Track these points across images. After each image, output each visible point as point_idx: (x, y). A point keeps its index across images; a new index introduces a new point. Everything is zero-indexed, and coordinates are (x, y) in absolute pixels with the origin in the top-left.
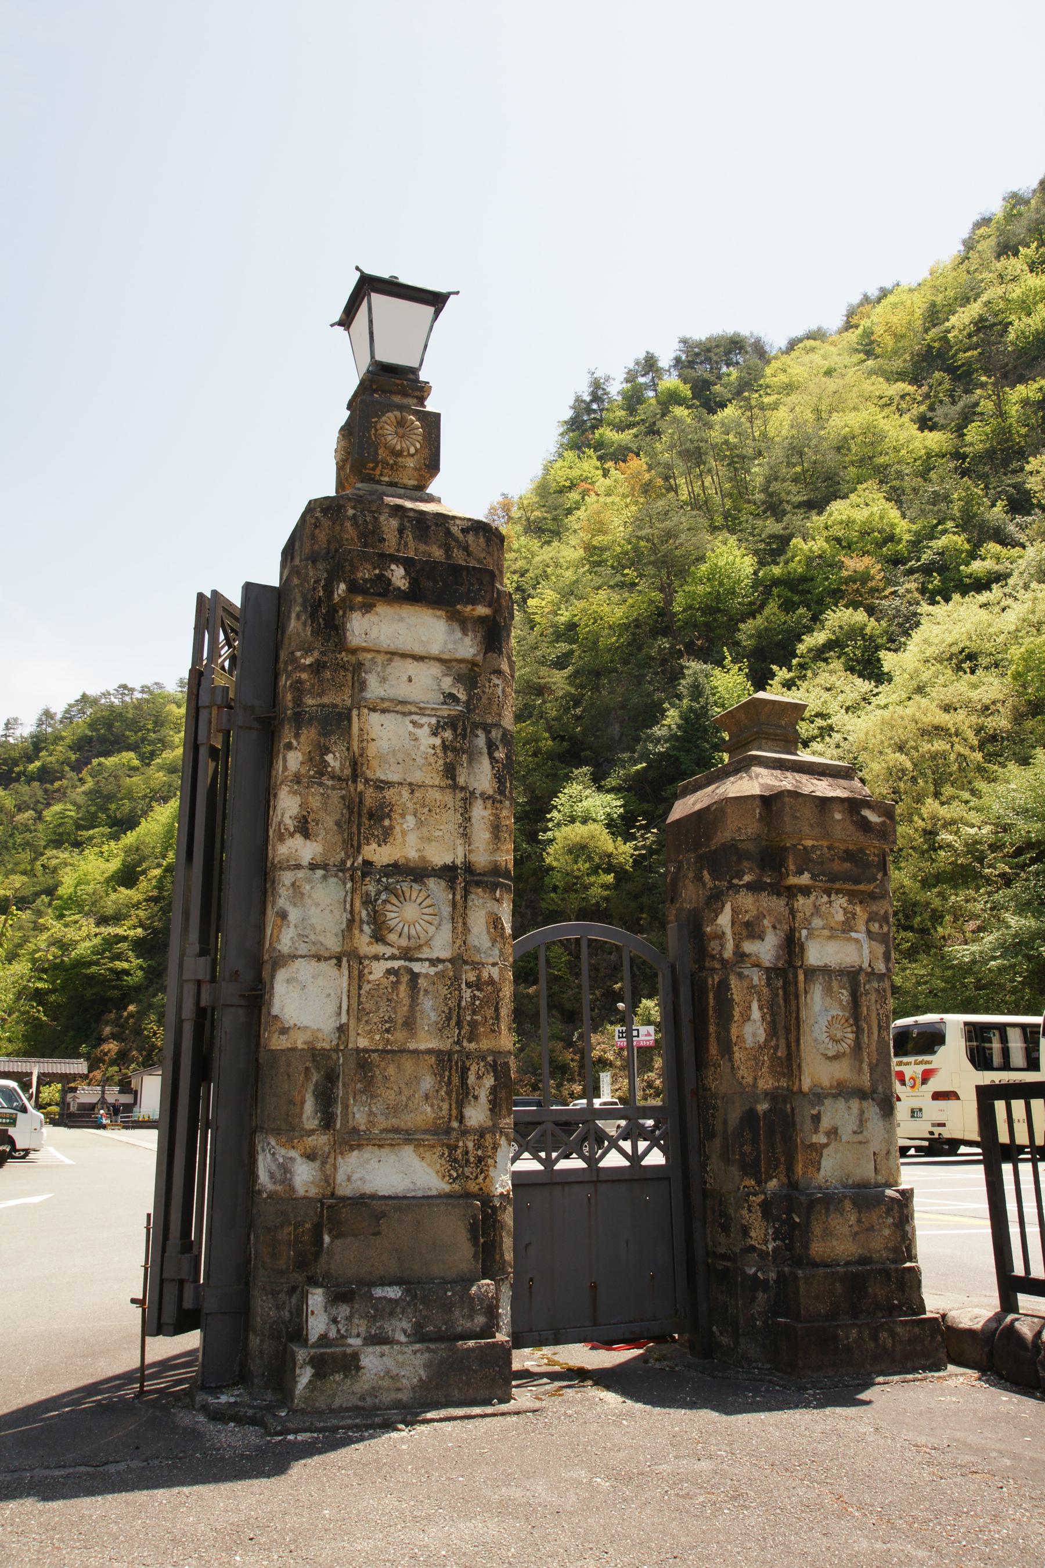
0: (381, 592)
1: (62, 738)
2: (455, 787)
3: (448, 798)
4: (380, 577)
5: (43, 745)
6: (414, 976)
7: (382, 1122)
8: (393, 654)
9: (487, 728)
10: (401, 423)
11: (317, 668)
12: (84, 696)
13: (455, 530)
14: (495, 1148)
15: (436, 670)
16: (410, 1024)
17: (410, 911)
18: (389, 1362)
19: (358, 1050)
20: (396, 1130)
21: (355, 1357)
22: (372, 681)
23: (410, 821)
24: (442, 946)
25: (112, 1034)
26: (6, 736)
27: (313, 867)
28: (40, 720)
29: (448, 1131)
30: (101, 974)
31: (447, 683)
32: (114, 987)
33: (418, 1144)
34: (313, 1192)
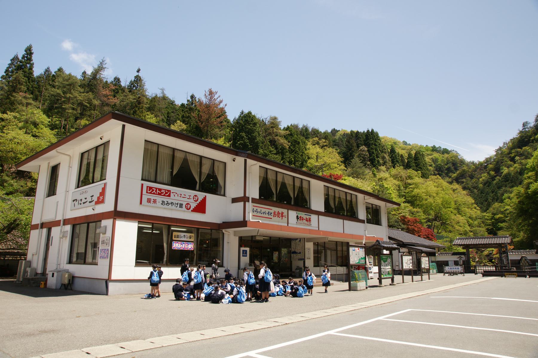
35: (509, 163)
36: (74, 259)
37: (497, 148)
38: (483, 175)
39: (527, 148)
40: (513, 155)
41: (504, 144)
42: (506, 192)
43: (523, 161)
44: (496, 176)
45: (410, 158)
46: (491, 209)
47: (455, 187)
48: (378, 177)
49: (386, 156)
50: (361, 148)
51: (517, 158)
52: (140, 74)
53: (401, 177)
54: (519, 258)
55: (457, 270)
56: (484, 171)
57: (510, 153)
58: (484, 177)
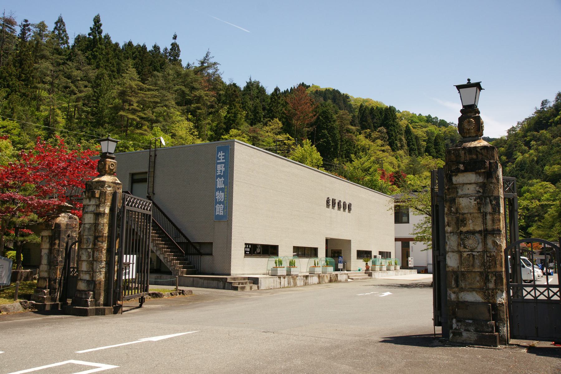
0: (458, 171)
2: (481, 212)
3: (479, 215)
4: (458, 168)
6: (474, 255)
7: (468, 287)
8: (464, 184)
9: (489, 197)
10: (469, 122)
11: (448, 189)
13: (478, 150)
14: (496, 293)
15: (474, 186)
16: (473, 266)
17: (470, 241)
18: (468, 335)
19: (462, 271)
20: (471, 288)
21: (461, 333)
22: (460, 191)
23: (471, 221)
24: (480, 248)
26: (543, 108)
27: (451, 233)
28: (557, 98)
29: (483, 289)
31: (477, 188)
33: (476, 292)
34: (455, 300)
35: (524, 147)
37: (509, 127)
39: (544, 132)
40: (528, 139)
41: (518, 124)
43: (540, 147)
44: (507, 162)
45: (430, 142)
48: (147, 73)
51: (533, 143)
52: (178, 41)
57: (525, 136)
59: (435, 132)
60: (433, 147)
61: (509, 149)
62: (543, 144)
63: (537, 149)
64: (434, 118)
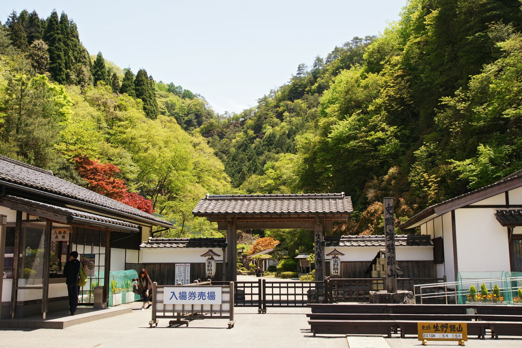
1: (327, 70)
5: (318, 75)
12: (336, 48)
25: (376, 196)
30: (360, 146)
32: (373, 157)
35: (276, 120)
36: (264, 261)
38: (237, 134)
39: (299, 101)
41: (271, 93)
42: (269, 158)
43: (294, 119)
44: (255, 138)
46: (246, 183)
47: (196, 140)
49: (84, 68)
50: (36, 42)
51: (286, 114)
53: (105, 104)
54: (370, 257)
55: (207, 303)
56: (241, 128)
58: (239, 137)
59: (177, 104)
60: (133, 87)
61: (258, 121)
62: (298, 115)
63: (290, 122)
64: (177, 88)
